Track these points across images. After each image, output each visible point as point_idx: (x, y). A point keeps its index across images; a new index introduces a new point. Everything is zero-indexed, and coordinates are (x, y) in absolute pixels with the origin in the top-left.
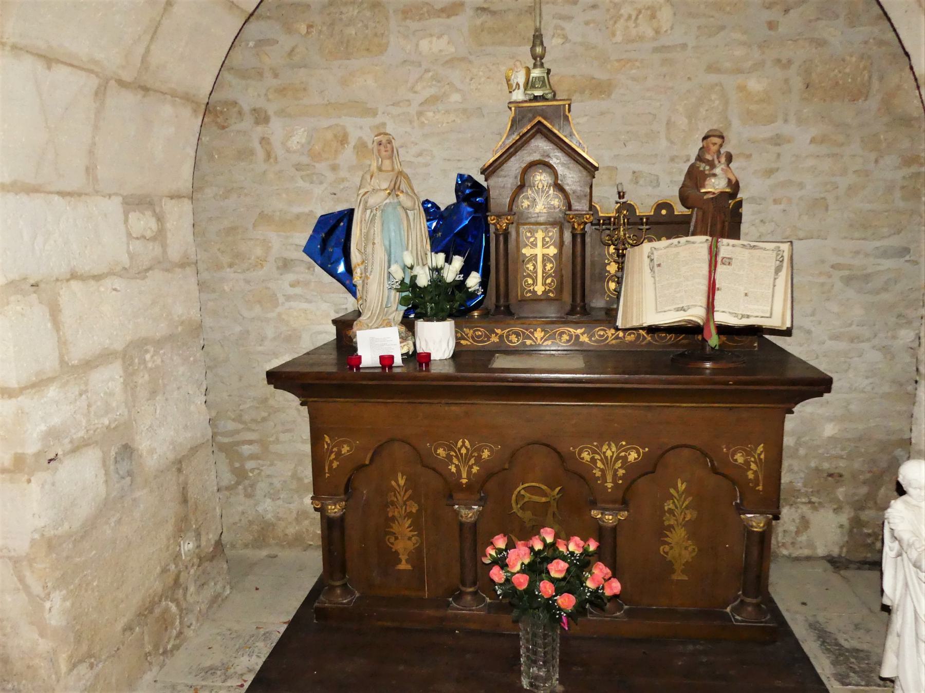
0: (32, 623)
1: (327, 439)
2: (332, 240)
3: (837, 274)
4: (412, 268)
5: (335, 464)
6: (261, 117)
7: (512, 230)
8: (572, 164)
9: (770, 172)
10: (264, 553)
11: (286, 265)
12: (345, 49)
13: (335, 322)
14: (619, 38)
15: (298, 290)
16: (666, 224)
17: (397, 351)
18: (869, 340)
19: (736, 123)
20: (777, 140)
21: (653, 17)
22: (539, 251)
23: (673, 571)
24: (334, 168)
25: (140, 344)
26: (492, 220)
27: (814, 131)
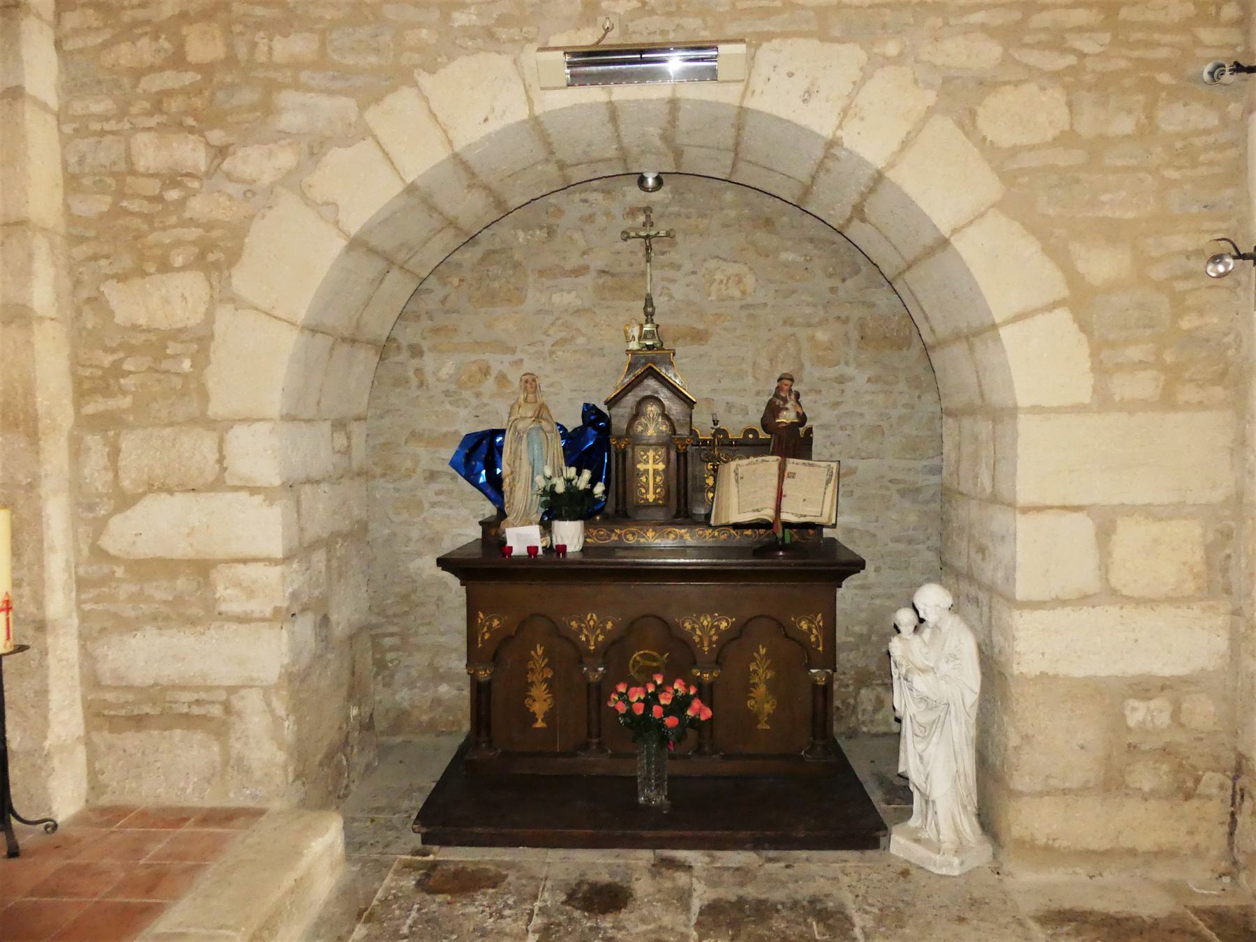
0: (272, 738)
1: (481, 615)
2: (480, 455)
3: (894, 487)
4: (550, 478)
5: (487, 636)
6: (416, 351)
7: (629, 450)
8: (676, 400)
9: (836, 405)
10: (399, 739)
11: (432, 476)
12: (491, 298)
13: (481, 523)
14: (713, 297)
15: (442, 498)
16: (750, 446)
17: (539, 543)
18: (923, 542)
19: (807, 365)
20: (841, 380)
21: (739, 282)
22: (650, 467)
23: (759, 722)
24: (478, 395)
25: (335, 535)
26: (613, 442)
27: (869, 373)
